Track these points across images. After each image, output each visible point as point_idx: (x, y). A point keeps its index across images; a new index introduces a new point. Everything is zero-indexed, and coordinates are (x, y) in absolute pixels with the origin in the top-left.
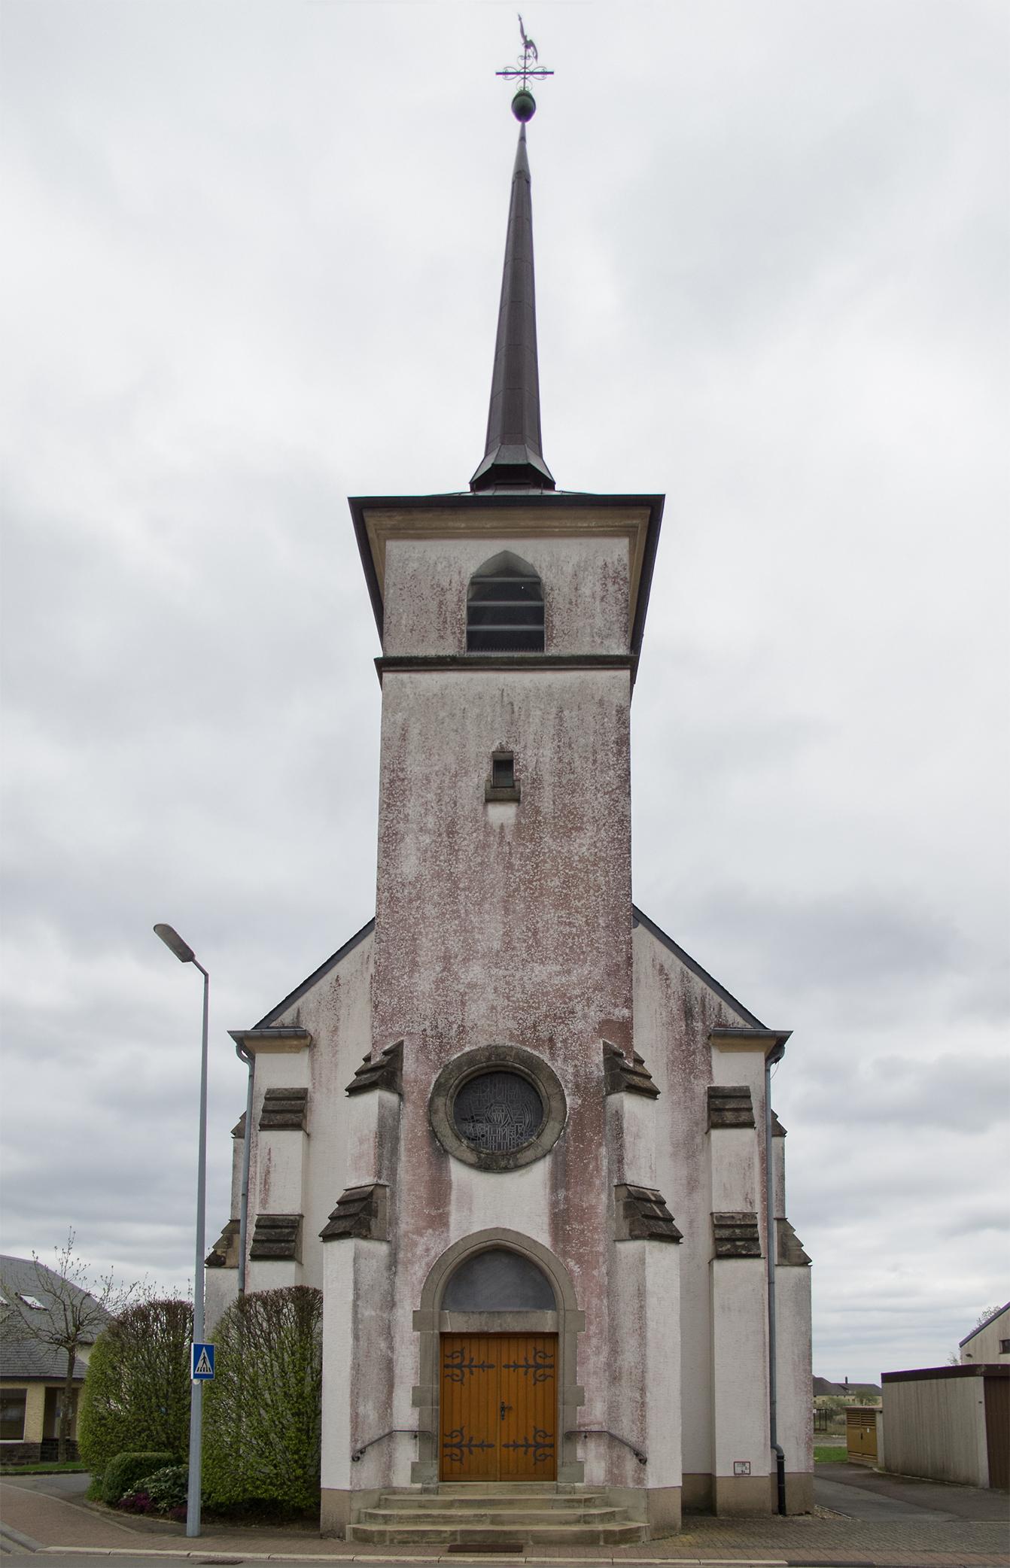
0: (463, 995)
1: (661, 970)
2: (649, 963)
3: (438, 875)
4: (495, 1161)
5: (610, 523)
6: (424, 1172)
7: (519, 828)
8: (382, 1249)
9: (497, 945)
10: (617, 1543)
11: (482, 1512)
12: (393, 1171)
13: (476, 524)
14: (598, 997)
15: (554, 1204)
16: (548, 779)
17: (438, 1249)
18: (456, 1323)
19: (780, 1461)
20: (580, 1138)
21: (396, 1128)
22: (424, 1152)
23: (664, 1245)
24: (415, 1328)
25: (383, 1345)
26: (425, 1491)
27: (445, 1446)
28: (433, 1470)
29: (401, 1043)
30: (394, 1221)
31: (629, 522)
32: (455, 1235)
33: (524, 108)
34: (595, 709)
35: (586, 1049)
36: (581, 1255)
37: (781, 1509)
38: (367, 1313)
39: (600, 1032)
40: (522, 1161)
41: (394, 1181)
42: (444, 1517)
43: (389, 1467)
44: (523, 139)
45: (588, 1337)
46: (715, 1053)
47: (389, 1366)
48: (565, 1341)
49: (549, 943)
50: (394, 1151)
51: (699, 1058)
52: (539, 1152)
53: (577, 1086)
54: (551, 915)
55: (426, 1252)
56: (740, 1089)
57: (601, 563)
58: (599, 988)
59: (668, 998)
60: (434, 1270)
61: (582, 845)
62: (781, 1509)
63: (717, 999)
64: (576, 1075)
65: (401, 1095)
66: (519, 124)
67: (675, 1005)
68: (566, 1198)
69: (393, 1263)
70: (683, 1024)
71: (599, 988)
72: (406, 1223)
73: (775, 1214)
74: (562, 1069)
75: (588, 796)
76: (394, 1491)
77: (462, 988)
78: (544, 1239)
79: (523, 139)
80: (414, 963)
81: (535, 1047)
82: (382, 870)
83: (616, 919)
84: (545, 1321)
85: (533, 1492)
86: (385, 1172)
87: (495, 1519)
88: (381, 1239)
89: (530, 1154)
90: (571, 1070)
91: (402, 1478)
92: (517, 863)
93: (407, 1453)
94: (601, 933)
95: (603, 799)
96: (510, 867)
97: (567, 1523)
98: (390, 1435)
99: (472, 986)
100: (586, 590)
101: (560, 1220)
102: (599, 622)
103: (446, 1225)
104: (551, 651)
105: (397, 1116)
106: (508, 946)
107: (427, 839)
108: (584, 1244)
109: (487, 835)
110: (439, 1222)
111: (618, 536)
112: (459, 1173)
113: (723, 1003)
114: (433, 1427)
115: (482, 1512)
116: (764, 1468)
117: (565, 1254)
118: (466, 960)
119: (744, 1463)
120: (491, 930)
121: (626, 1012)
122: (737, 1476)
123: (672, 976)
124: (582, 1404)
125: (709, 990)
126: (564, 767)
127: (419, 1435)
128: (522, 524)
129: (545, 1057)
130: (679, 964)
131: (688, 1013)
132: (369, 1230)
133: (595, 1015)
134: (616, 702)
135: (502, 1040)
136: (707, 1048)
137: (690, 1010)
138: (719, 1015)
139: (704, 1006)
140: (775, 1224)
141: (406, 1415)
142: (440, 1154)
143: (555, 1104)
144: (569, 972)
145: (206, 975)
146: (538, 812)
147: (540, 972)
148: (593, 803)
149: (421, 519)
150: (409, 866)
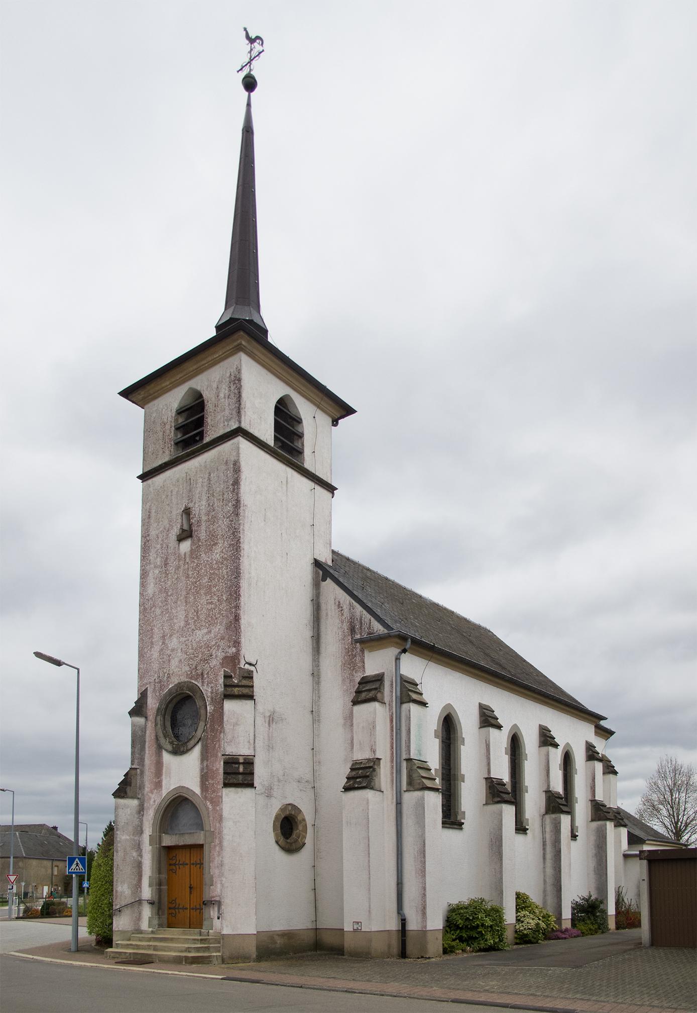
0: (169, 656)
1: (339, 605)
2: (333, 602)
3: (160, 591)
4: (179, 750)
5: (228, 348)
6: (153, 758)
7: (192, 551)
8: (135, 803)
9: (182, 624)
10: (192, 963)
11: (151, 943)
12: (142, 760)
13: (173, 380)
14: (222, 643)
15: (202, 770)
16: (204, 518)
17: (158, 801)
18: (168, 841)
19: (404, 922)
20: (213, 730)
21: (144, 736)
22: (154, 749)
23: (239, 790)
24: (150, 845)
25: (135, 854)
26: (152, 932)
27: (170, 908)
28: (156, 922)
29: (146, 689)
30: (142, 787)
31: (235, 344)
32: (164, 792)
33: (250, 84)
34: (224, 467)
35: (216, 675)
36: (212, 798)
37: (403, 954)
38: (123, 838)
39: (222, 665)
40: (189, 747)
41: (143, 765)
42: (137, 945)
43: (139, 918)
44: (249, 105)
45: (215, 846)
46: (366, 653)
47: (139, 865)
48: (206, 848)
49: (202, 617)
50: (143, 749)
51: (358, 658)
52: (197, 740)
53: (212, 698)
54: (204, 600)
55: (155, 800)
56: (378, 675)
57: (228, 375)
58: (223, 638)
59: (342, 622)
60: (157, 812)
61: (217, 554)
62: (403, 954)
63: (369, 616)
64: (212, 693)
65: (146, 718)
66: (247, 93)
67: (346, 626)
68: (207, 766)
69: (141, 810)
70: (350, 638)
71: (223, 638)
72: (148, 787)
73: (404, 756)
74: (206, 690)
75: (220, 522)
76: (141, 932)
77: (169, 652)
78: (197, 790)
79: (249, 105)
80: (152, 643)
81: (196, 680)
82: (141, 594)
83: (230, 594)
84: (199, 838)
85: (191, 935)
86: (136, 761)
87: (155, 948)
88: (132, 798)
89: (192, 742)
90: (210, 690)
91: (145, 925)
92: (190, 573)
93: (147, 912)
94: (224, 604)
95: (227, 521)
96: (188, 577)
97: (182, 951)
98: (140, 902)
99: (173, 650)
100: (222, 395)
101: (205, 777)
102: (227, 412)
103: (161, 786)
104: (207, 439)
105: (144, 729)
106: (187, 623)
107: (157, 571)
108: (214, 792)
109: (179, 561)
110: (158, 785)
111: (236, 353)
112: (167, 757)
113: (372, 619)
114: (156, 900)
115: (151, 943)
116: (393, 925)
117: (206, 798)
118: (171, 636)
119: (358, 923)
120: (180, 614)
121: (234, 650)
122: (355, 931)
123: (344, 608)
124: (212, 885)
125: (365, 612)
126: (211, 508)
127: (151, 903)
128: (191, 369)
129: (199, 685)
130: (348, 598)
131: (352, 630)
132: (126, 793)
133: (221, 655)
134: (233, 459)
135: (184, 679)
136: (362, 651)
137: (354, 627)
138: (369, 628)
139: (361, 623)
140: (404, 764)
141: (147, 892)
142: (160, 748)
143: (202, 712)
144: (210, 632)
145: (78, 669)
146: (199, 540)
147: (199, 634)
148: (222, 525)
149: (152, 388)
150: (151, 589)
